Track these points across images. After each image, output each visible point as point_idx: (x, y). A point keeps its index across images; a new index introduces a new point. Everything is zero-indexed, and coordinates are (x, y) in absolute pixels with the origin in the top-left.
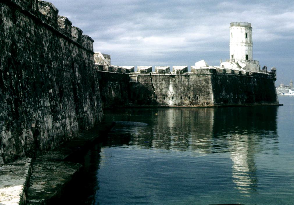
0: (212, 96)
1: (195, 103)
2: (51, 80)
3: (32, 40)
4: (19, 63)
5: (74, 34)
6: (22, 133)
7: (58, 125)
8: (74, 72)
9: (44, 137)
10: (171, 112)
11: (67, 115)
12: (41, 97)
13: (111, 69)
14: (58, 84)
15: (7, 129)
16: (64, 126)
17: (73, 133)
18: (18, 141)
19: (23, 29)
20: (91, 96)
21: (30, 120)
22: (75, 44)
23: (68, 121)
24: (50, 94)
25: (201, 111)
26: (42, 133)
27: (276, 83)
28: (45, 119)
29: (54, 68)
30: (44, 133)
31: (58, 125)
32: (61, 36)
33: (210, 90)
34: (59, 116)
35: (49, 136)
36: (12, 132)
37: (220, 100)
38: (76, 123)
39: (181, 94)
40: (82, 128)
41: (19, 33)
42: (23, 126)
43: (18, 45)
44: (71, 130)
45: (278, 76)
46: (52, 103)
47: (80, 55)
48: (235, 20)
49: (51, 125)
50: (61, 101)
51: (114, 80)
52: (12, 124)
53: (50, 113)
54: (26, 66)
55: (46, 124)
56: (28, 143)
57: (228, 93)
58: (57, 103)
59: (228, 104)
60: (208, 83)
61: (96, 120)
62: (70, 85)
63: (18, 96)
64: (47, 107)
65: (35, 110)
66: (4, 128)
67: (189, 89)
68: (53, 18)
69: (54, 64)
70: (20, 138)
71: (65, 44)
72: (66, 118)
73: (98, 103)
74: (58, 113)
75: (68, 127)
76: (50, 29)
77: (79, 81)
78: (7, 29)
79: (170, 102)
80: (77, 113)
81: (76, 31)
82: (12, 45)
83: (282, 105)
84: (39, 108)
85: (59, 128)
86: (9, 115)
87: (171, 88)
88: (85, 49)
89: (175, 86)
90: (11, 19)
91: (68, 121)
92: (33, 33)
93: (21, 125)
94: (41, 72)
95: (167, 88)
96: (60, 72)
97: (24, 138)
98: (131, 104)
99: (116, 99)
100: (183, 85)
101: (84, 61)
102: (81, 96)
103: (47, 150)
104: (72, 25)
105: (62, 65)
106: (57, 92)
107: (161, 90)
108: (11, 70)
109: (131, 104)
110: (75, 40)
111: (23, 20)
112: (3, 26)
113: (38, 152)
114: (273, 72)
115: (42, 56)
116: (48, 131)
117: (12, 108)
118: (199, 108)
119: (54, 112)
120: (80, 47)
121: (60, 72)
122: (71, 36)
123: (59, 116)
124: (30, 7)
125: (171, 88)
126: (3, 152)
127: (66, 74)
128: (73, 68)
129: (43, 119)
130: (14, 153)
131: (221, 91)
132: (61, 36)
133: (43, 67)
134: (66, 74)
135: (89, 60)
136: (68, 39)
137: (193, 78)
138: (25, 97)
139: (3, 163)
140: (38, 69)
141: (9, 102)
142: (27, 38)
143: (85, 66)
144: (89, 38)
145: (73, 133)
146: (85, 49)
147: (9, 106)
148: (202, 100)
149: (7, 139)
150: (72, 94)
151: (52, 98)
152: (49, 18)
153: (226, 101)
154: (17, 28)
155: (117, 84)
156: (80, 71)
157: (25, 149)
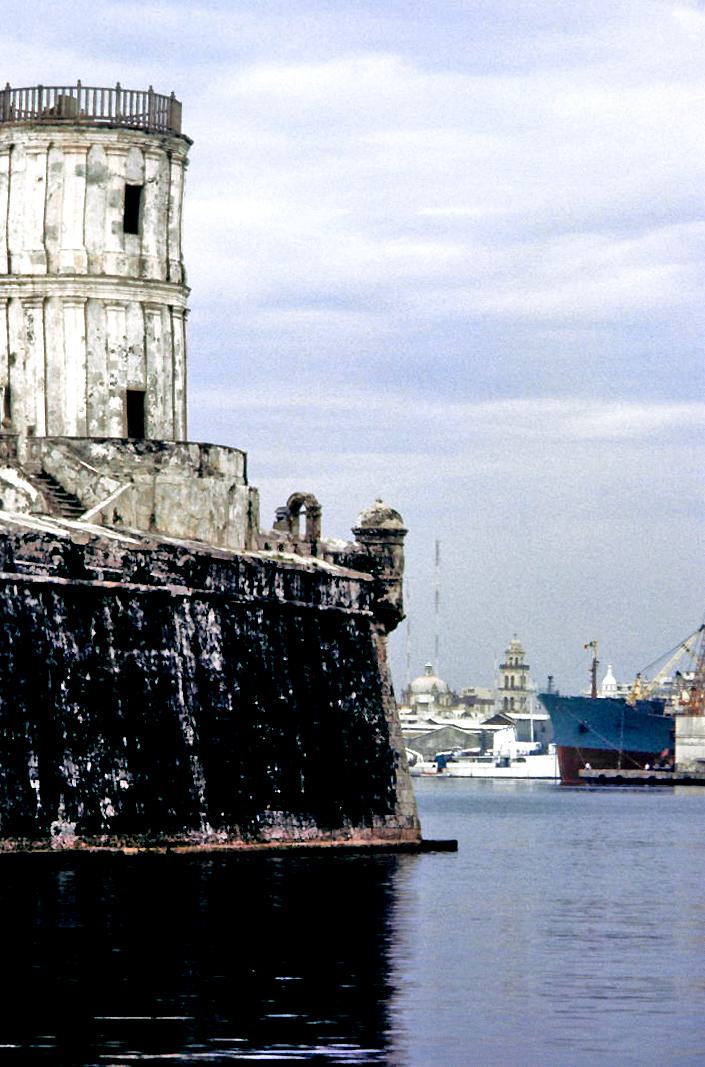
45: (414, 588)
83: (450, 846)
114: (379, 547)
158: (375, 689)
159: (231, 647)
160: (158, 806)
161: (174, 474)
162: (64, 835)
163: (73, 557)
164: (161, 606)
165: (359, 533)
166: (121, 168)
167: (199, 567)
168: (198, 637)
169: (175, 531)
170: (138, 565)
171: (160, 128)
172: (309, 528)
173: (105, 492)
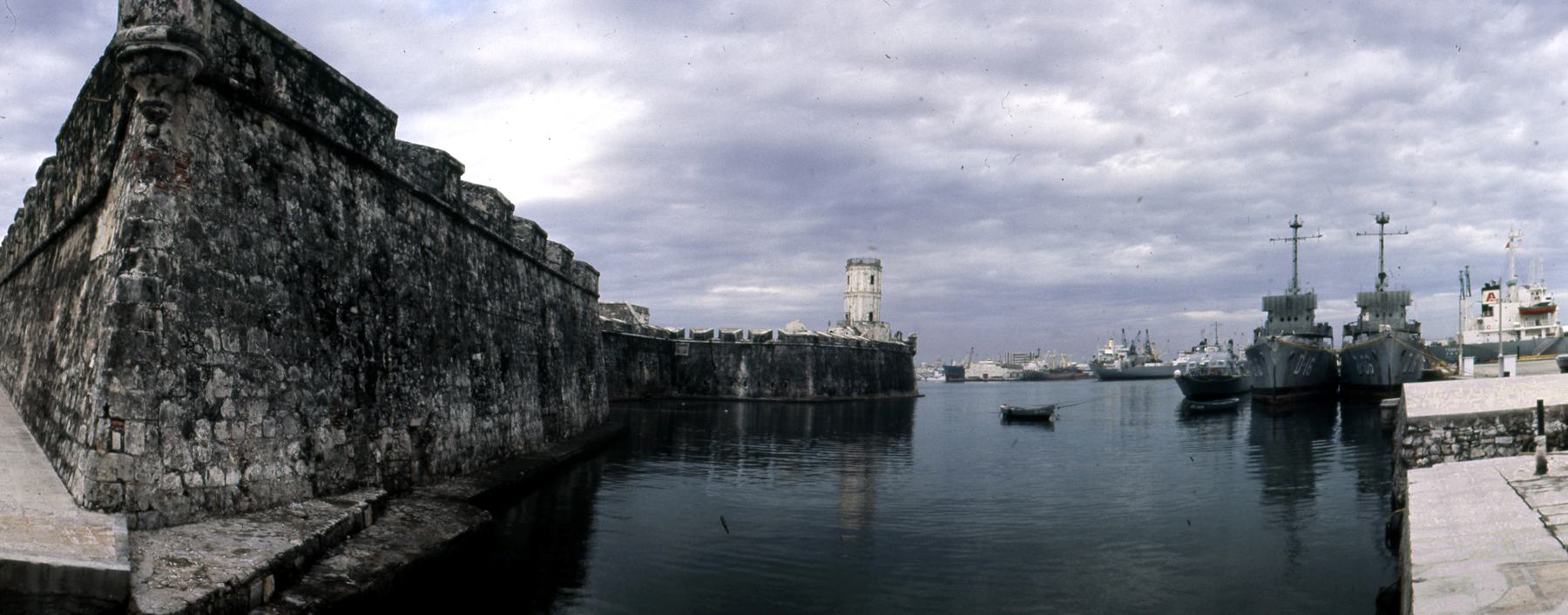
0: (811, 383)
1: (782, 394)
2: (482, 337)
3: (437, 253)
4: (393, 293)
5: (554, 257)
6: (380, 437)
7: (488, 424)
8: (545, 326)
9: (444, 448)
10: (741, 407)
11: (515, 407)
12: (446, 366)
13: (647, 331)
14: (498, 343)
15: (336, 424)
16: (504, 428)
17: (527, 442)
18: (362, 450)
19: (414, 228)
20: (581, 372)
21: (408, 412)
22: (553, 274)
23: (516, 418)
24: (473, 362)
25: (791, 407)
26: (439, 440)
27: (915, 360)
28: (453, 412)
29: (491, 312)
30: (445, 438)
31: (488, 424)
32: (520, 255)
33: (808, 372)
34: (495, 408)
35: (459, 446)
36: (348, 431)
37: (824, 390)
38: (539, 424)
39: (755, 379)
40: (551, 433)
41: (403, 235)
42: (383, 422)
43: (396, 257)
44: (523, 435)
45: (918, 349)
46: (477, 381)
47: (564, 297)
48: (855, 255)
49: (468, 424)
50: (503, 378)
51: (648, 350)
52: (351, 414)
53: (470, 400)
54: (410, 300)
55: (454, 423)
56: (394, 456)
57: (835, 375)
58: (493, 381)
59: (835, 398)
60: (803, 358)
61: (589, 421)
62: (531, 349)
63: (378, 358)
64: (461, 388)
65: (426, 392)
66: (327, 421)
67: (772, 368)
68: (501, 218)
69: (494, 306)
70: (371, 445)
71: (528, 272)
72: (512, 413)
73: (598, 387)
74: (488, 400)
75: (516, 431)
76: (490, 238)
77: (556, 344)
78: (365, 222)
79: (741, 392)
80: (543, 404)
81: (559, 252)
82: (375, 256)
84: (438, 388)
85: (490, 431)
86: (345, 395)
87: (743, 367)
88: (577, 287)
89: (750, 364)
90: (381, 204)
91: (516, 418)
92: (443, 239)
93: (378, 418)
94: (456, 317)
95: (737, 366)
96: (507, 324)
97: (384, 447)
98: (675, 393)
99: (651, 383)
100: (763, 362)
101: (573, 309)
102: (557, 372)
103: (452, 475)
104: (549, 239)
105: (515, 309)
106: (495, 358)
107: (727, 369)
108: (367, 307)
109: (675, 393)
110: (555, 268)
111: (414, 212)
112: (357, 214)
113: (426, 477)
114: (912, 341)
115: (463, 287)
116: (458, 436)
117: (357, 383)
118: (788, 402)
119: (481, 400)
120: (565, 281)
121: (507, 324)
122: (544, 258)
123: (495, 408)
124: (441, 188)
125: (743, 367)
126: (312, 471)
127: (522, 328)
128: (543, 316)
129: (448, 411)
130: (350, 476)
131: (824, 375)
132: (520, 255)
133: (460, 307)
134: (522, 328)
135: (586, 307)
136: (536, 263)
137: (780, 350)
138: (400, 363)
139: (309, 493)
140: (446, 310)
141: (348, 368)
142: (423, 247)
143: (574, 318)
144: (589, 268)
145: (527, 442)
146: (577, 287)
147: (348, 377)
148: (793, 390)
149: (331, 445)
150: (534, 367)
151: (476, 370)
152: (491, 217)
153: (832, 392)
154: (397, 225)
155: (654, 357)
156: (561, 324)
157: (383, 470)
158: (911, 366)
159: (886, 359)
160: (871, 390)
161: (877, 328)
162: (855, 395)
163: (858, 343)
164: (873, 351)
165: (1270, 305)
166: (870, 272)
167: (881, 345)
168: (880, 359)
169: (877, 339)
170: (870, 344)
171: (877, 265)
172: (1126, 234)
173: (865, 331)
